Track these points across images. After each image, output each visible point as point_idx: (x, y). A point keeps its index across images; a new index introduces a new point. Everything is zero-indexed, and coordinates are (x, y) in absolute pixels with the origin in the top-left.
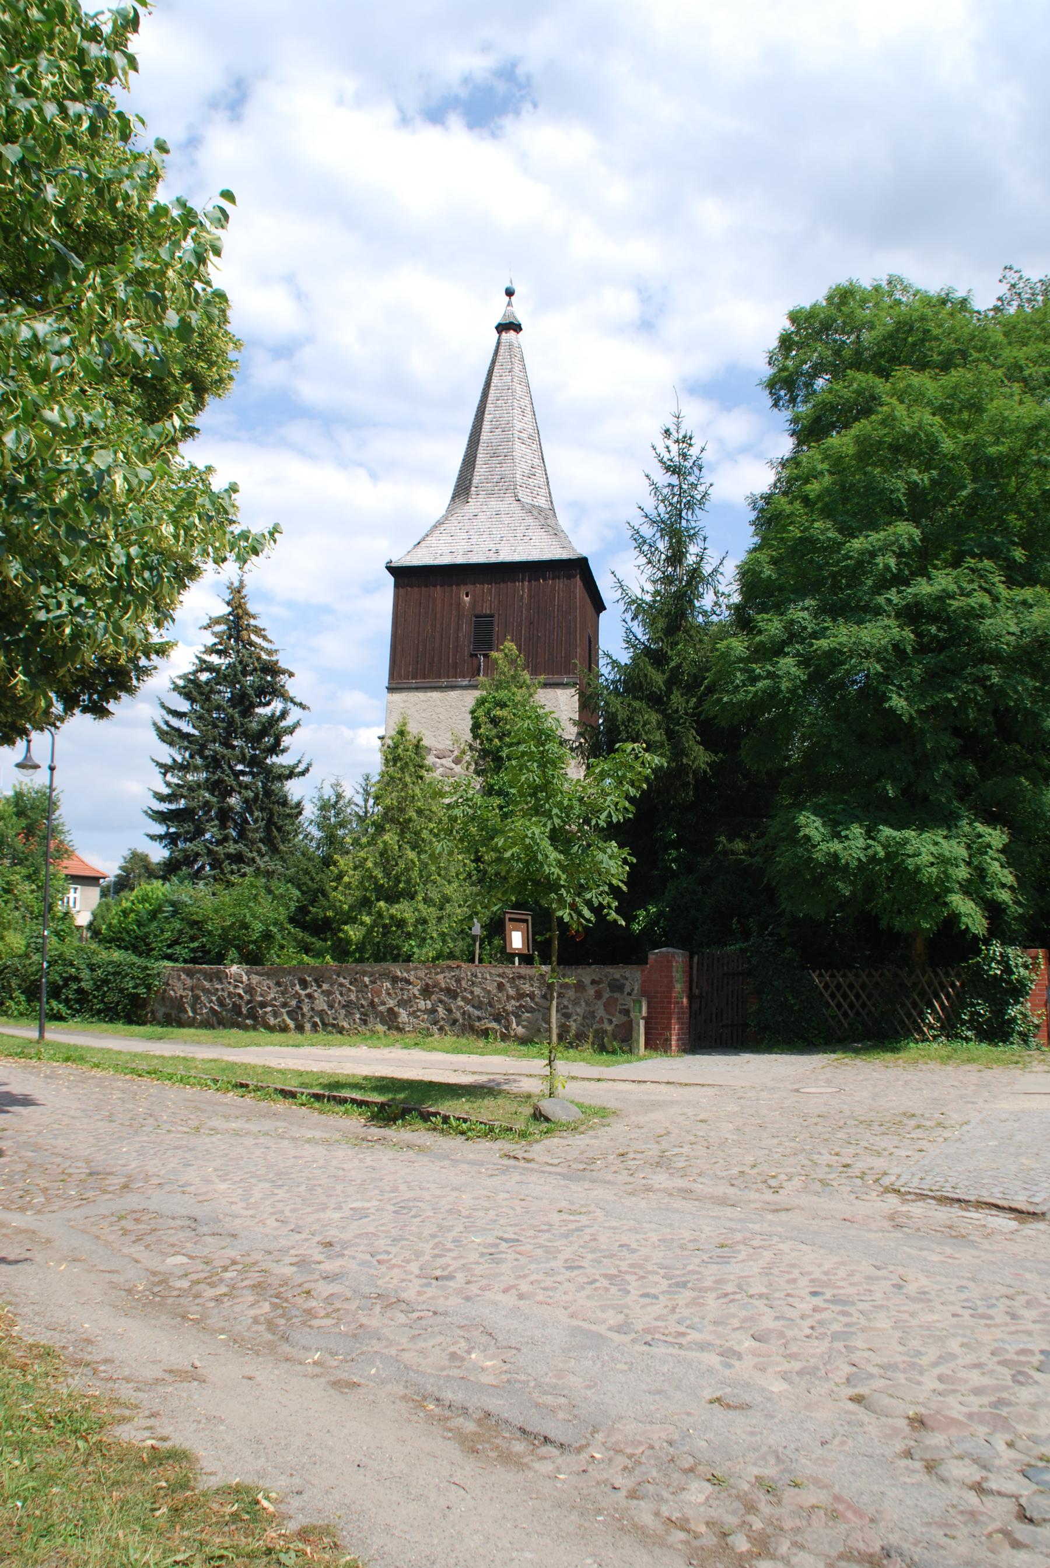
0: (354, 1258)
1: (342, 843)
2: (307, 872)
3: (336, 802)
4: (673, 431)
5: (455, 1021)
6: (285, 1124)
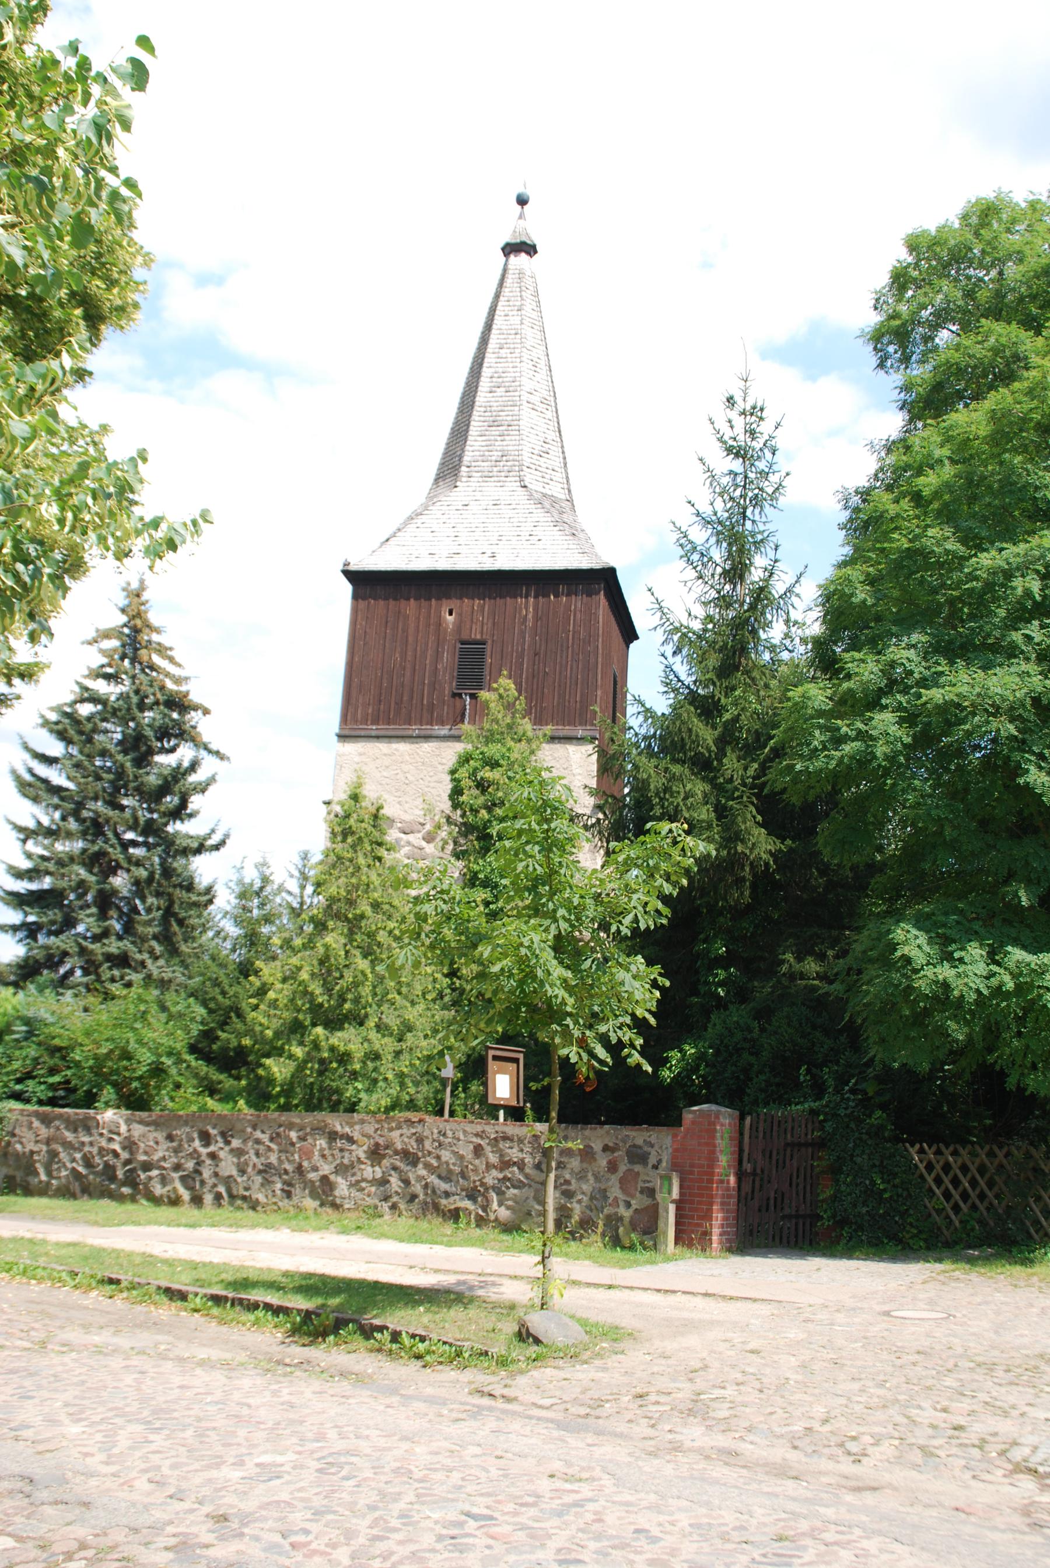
0: (257, 1539)
1: (266, 945)
2: (216, 983)
3: (262, 888)
4: (738, 398)
5: (413, 1197)
6: (170, 1339)
